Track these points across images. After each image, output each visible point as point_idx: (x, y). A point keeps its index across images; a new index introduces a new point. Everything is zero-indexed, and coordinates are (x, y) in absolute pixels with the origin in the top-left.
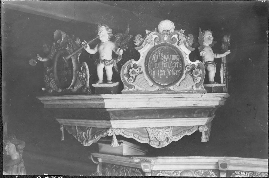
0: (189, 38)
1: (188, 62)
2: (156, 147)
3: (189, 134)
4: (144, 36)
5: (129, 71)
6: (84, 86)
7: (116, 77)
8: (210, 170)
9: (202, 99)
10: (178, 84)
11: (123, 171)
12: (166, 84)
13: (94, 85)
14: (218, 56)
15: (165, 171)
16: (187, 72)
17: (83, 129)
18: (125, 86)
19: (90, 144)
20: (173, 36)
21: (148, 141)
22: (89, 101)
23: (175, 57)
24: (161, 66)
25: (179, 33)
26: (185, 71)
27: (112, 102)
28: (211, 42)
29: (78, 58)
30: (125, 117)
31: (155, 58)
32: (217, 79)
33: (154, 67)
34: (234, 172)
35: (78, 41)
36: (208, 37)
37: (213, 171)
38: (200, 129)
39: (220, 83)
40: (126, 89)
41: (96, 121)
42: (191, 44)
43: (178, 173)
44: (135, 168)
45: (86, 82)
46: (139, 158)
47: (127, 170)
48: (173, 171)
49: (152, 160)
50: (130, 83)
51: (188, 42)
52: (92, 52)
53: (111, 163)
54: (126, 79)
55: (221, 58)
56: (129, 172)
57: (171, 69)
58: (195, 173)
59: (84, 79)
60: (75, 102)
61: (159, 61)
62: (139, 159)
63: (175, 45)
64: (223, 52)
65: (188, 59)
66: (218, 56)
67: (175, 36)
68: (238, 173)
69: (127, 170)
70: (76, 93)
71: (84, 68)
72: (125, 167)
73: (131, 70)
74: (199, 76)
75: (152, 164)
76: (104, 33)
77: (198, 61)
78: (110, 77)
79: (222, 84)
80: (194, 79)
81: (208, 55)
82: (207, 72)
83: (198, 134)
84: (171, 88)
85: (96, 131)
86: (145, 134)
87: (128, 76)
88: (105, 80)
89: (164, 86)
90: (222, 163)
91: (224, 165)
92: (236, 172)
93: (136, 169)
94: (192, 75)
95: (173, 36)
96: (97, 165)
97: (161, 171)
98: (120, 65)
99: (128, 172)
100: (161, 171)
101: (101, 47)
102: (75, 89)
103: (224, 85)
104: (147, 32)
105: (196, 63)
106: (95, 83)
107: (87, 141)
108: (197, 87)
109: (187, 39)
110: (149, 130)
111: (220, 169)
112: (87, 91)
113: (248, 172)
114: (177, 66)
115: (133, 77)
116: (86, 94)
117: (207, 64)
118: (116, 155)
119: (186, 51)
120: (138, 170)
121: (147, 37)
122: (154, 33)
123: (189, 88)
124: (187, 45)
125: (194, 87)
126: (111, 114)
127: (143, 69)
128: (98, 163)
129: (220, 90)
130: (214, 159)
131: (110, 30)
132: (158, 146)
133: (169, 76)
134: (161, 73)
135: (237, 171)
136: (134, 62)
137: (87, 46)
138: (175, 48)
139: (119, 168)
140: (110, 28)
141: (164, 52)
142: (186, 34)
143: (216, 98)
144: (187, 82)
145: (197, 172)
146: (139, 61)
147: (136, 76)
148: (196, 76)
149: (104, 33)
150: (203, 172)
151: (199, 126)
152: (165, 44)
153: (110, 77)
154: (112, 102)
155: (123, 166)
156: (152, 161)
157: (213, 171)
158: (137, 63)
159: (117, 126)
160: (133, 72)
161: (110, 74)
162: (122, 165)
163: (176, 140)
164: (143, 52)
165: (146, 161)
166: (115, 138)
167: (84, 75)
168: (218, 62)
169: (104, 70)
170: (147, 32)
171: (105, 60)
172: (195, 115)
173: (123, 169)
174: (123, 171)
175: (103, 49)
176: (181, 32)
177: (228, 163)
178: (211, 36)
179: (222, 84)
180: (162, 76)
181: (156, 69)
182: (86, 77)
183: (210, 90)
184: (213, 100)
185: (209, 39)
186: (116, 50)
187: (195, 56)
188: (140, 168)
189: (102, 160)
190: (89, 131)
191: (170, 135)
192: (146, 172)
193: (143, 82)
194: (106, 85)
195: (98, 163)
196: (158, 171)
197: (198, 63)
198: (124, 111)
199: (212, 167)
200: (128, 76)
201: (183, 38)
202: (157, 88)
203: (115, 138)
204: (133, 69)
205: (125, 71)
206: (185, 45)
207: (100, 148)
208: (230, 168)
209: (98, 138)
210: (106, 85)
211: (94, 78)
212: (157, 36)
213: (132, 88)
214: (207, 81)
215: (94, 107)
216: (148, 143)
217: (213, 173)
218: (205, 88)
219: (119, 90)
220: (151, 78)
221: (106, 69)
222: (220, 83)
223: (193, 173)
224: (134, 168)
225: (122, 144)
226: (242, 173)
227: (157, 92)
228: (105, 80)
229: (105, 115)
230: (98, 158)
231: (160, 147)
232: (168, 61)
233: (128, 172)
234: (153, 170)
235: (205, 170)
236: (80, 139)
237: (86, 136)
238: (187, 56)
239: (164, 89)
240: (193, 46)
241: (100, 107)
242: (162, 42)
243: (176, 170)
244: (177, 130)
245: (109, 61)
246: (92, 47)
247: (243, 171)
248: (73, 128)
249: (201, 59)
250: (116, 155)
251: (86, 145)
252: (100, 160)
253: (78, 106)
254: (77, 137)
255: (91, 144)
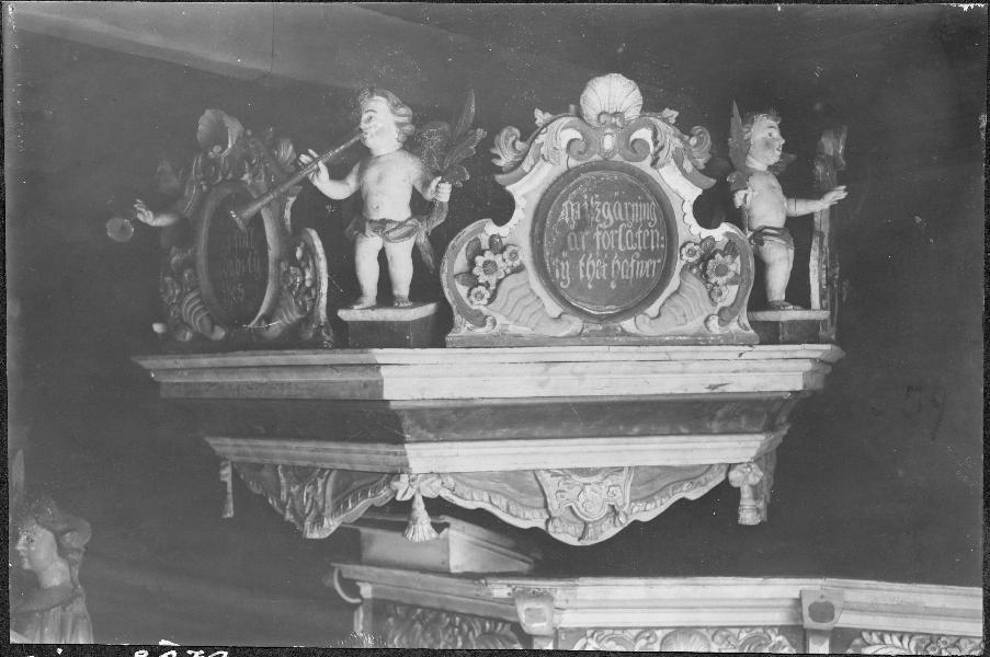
0: (693, 141)
1: (689, 228)
2: (573, 541)
3: (693, 495)
4: (529, 132)
5: (472, 264)
6: (309, 317)
7: (426, 284)
8: (772, 627)
9: (740, 365)
10: (653, 310)
11: (450, 631)
12: (610, 310)
13: (343, 314)
14: (801, 208)
15: (606, 632)
16: (688, 267)
17: (303, 475)
18: (458, 318)
19: (329, 529)
20: (636, 135)
21: (544, 521)
22: (325, 372)
23: (645, 211)
24: (592, 242)
25: (659, 123)
26: (679, 265)
27: (408, 377)
28: (774, 156)
29: (287, 214)
30: (457, 430)
31: (568, 213)
32: (797, 292)
33: (565, 247)
34: (861, 636)
35: (286, 152)
36: (764, 138)
37: (783, 630)
38: (734, 476)
39: (807, 306)
40: (463, 328)
41: (354, 447)
42: (701, 162)
43: (651, 640)
44: (495, 621)
45: (315, 301)
46: (511, 582)
47: (465, 627)
48: (638, 631)
49: (558, 588)
50: (479, 305)
51: (691, 158)
52: (336, 191)
53: (407, 601)
54: (463, 290)
55: (811, 216)
56: (474, 634)
57: (629, 254)
58: (718, 638)
59: (308, 291)
60: (275, 377)
61: (583, 224)
62: (509, 585)
63: (645, 166)
64: (817, 194)
65: (691, 219)
66: (801, 208)
67: (644, 134)
68: (875, 638)
69: (465, 627)
70: (279, 345)
71: (310, 251)
72: (459, 614)
73: (480, 260)
74: (732, 282)
75: (557, 604)
76: (382, 122)
77: (725, 227)
78: (402, 285)
79: (817, 312)
80: (713, 293)
81: (765, 204)
82: (762, 267)
83: (726, 495)
84: (628, 324)
85: (350, 484)
86: (531, 493)
87: (471, 280)
88: (386, 295)
89: (600, 319)
90: (815, 603)
91: (824, 611)
92: (865, 635)
93: (500, 625)
94: (704, 276)
95: (636, 135)
96: (356, 606)
97: (589, 633)
98: (440, 241)
99: (471, 634)
100: (589, 633)
101: (372, 174)
102: (276, 326)
103: (824, 315)
104: (540, 117)
105: (721, 232)
106: (348, 305)
107: (319, 520)
108: (723, 322)
109: (686, 143)
110: (546, 478)
111: (809, 623)
112: (317, 334)
113: (912, 635)
114: (648, 243)
115: (487, 285)
116: (316, 345)
117: (759, 235)
118: (424, 570)
119: (683, 191)
120: (507, 627)
121: (541, 138)
122: (565, 120)
123: (693, 326)
124: (688, 165)
125: (714, 322)
126: (407, 422)
127: (526, 256)
128: (357, 601)
129: (807, 333)
130: (784, 589)
131: (403, 111)
132: (580, 539)
133: (619, 282)
134: (592, 269)
135: (870, 632)
136: (491, 228)
137: (318, 170)
138: (643, 177)
139: (437, 620)
140: (405, 103)
141: (604, 191)
142: (684, 127)
143: (792, 364)
144: (687, 305)
145: (724, 633)
146: (510, 224)
147: (499, 282)
148: (721, 280)
149: (382, 122)
150: (743, 635)
151: (730, 467)
152: (605, 165)
153: (402, 285)
154: (408, 377)
155: (452, 614)
156: (559, 592)
157: (783, 630)
158: (503, 231)
159: (431, 465)
160: (490, 267)
161: (403, 274)
162: (449, 607)
163: (646, 517)
164: (526, 191)
165: (534, 592)
166: (420, 509)
167: (308, 275)
168: (798, 230)
169: (383, 258)
170: (540, 117)
171: (384, 222)
172: (715, 426)
173: (452, 624)
174: (450, 631)
175: (380, 179)
176: (665, 120)
177: (836, 603)
178: (776, 134)
179: (817, 312)
180: (594, 281)
181: (575, 256)
182: (316, 283)
183: (770, 334)
184: (783, 371)
185: (768, 145)
186: (426, 184)
187: (716, 206)
188: (512, 619)
189: (374, 591)
190: (325, 485)
191: (622, 497)
192: (536, 636)
193: (523, 303)
194: (388, 315)
195: (357, 601)
196: (579, 629)
197: (727, 234)
198: (456, 410)
199: (779, 618)
200: (471, 280)
201: (672, 141)
202: (575, 324)
203: (420, 509)
204: (489, 256)
205: (460, 263)
206: (681, 167)
207: (365, 544)
208: (845, 620)
209: (358, 508)
210: (388, 315)
211: (346, 287)
212: (578, 136)
213: (483, 324)
214: (759, 298)
215: (344, 394)
216: (542, 526)
217: (780, 638)
218: (754, 324)
219: (436, 333)
220: (553, 289)
221: (382, 255)
222: (807, 306)
223: (709, 637)
224: (490, 619)
225: (446, 530)
226: (887, 638)
227: (577, 338)
228: (386, 295)
229: (383, 423)
230: (359, 584)
231: (587, 542)
232: (617, 224)
233: (471, 634)
234: (562, 628)
235: (753, 627)
236: (293, 511)
237: (315, 503)
238: (688, 209)
239: (603, 331)
240: (707, 171)
241: (366, 394)
242: (596, 157)
243: (647, 629)
244: (648, 480)
245: (401, 224)
246: (337, 174)
247: (891, 633)
248: (265, 473)
249: (738, 217)
250: (424, 570)
251: (316, 536)
252: (366, 591)
253: (285, 393)
254: (283, 505)
255: (333, 529)
